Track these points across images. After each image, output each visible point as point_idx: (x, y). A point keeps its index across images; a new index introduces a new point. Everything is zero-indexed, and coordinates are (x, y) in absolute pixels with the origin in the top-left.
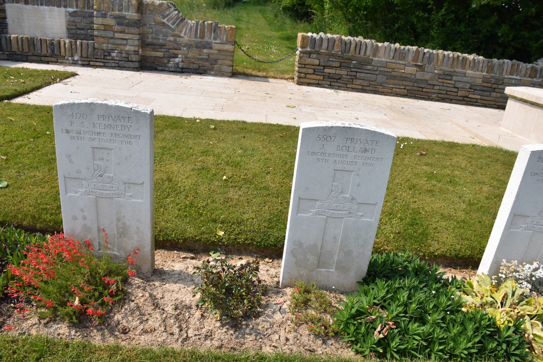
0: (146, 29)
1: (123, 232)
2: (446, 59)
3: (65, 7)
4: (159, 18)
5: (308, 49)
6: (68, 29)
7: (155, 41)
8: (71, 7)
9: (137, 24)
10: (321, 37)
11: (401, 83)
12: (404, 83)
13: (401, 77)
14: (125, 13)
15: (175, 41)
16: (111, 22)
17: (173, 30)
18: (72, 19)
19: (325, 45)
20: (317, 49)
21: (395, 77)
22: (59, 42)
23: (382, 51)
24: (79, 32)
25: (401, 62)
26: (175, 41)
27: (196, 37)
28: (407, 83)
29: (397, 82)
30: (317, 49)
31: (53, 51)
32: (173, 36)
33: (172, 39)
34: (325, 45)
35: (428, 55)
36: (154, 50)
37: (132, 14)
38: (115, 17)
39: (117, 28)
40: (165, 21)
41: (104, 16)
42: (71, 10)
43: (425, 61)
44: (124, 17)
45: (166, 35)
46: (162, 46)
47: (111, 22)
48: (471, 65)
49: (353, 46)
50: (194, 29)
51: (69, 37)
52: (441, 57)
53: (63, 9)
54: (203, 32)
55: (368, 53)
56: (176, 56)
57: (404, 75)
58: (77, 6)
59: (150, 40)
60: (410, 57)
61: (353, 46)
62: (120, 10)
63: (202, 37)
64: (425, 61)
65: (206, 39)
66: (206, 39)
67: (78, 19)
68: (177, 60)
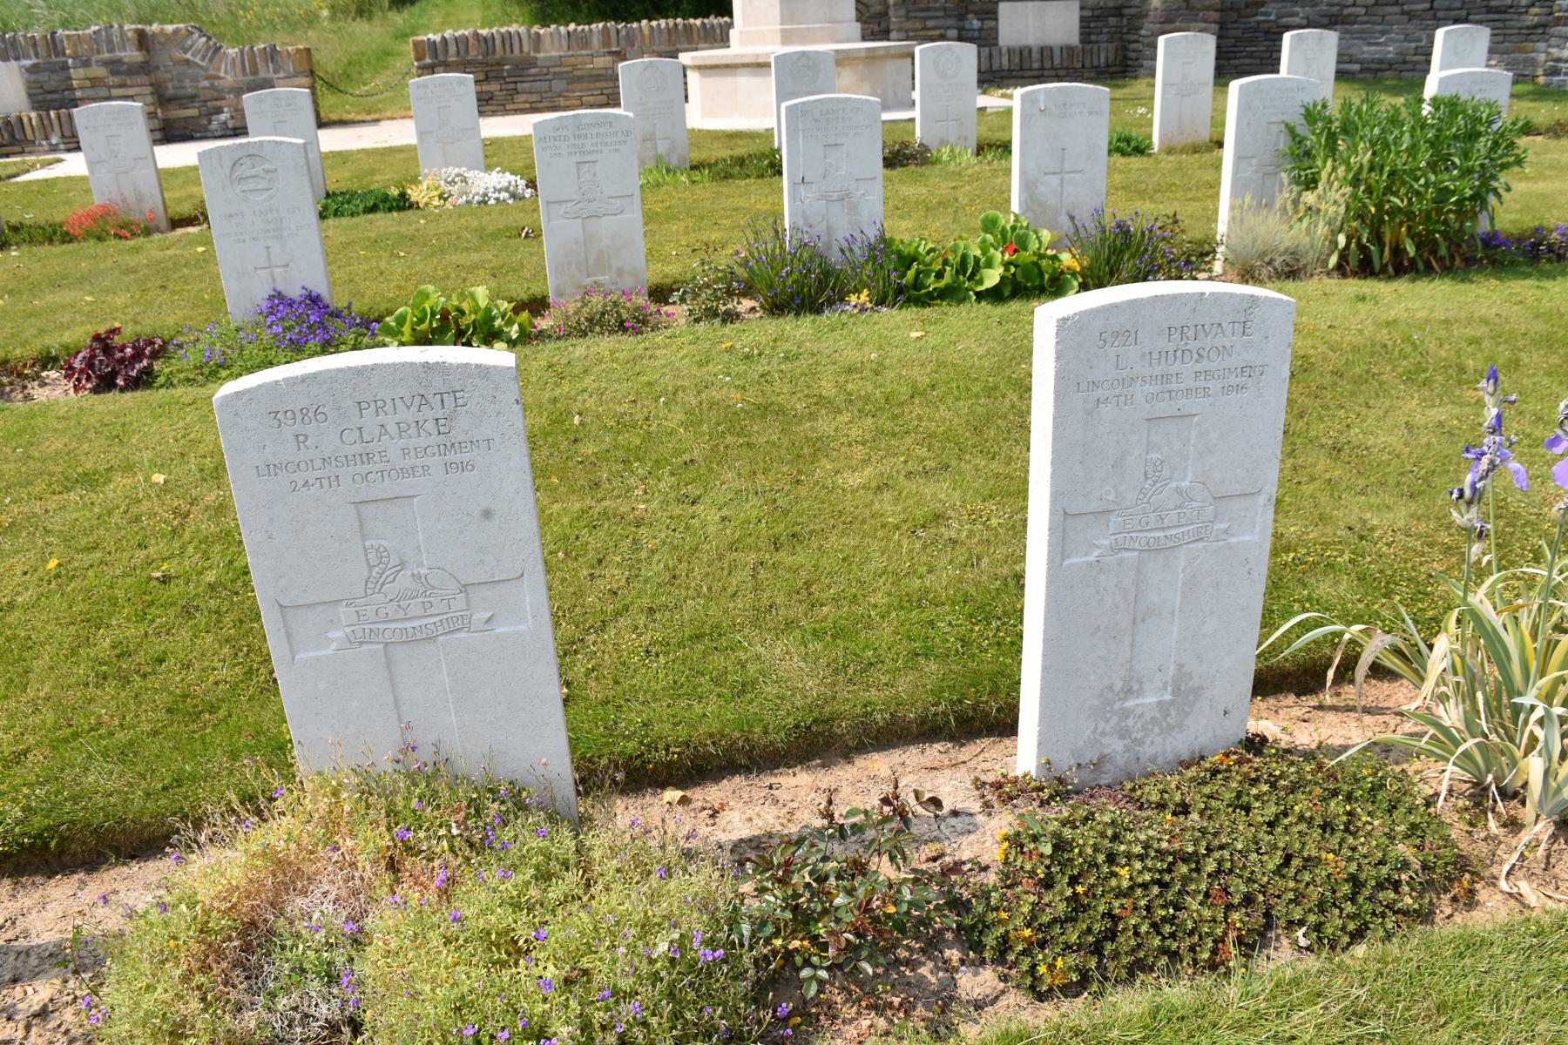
0: (161, 75)
1: (140, 199)
2: (656, 34)
3: (17, 59)
4: (178, 54)
5: (428, 60)
6: (30, 95)
7: (180, 93)
8: (27, 57)
9: (145, 68)
10: (444, 38)
11: (592, 85)
12: (598, 84)
13: (590, 76)
14: (119, 54)
15: (212, 87)
16: (101, 72)
17: (205, 69)
18: (33, 77)
19: (452, 49)
20: (441, 57)
21: (580, 79)
22: (20, 119)
23: (547, 43)
24: (49, 97)
25: (583, 52)
26: (212, 87)
27: (244, 73)
28: (604, 84)
29: (585, 85)
30: (441, 57)
31: (13, 135)
32: (207, 78)
33: (206, 83)
34: (452, 49)
35: (623, 33)
36: (181, 107)
37: (132, 55)
38: (106, 63)
39: (111, 80)
40: (188, 56)
41: (86, 64)
42: (28, 63)
43: (623, 42)
44: (119, 61)
45: (195, 79)
46: (193, 98)
47: (101, 72)
48: (702, 34)
49: (498, 42)
50: (238, 62)
51: (34, 109)
52: (646, 31)
53: (13, 63)
54: (254, 65)
55: (526, 49)
56: (219, 111)
57: (595, 73)
58: (37, 55)
59: (170, 92)
60: (596, 42)
61: (498, 42)
62: (111, 51)
63: (255, 72)
64: (623, 42)
65: (262, 74)
66: (262, 74)
67: (43, 77)
68: (222, 117)
